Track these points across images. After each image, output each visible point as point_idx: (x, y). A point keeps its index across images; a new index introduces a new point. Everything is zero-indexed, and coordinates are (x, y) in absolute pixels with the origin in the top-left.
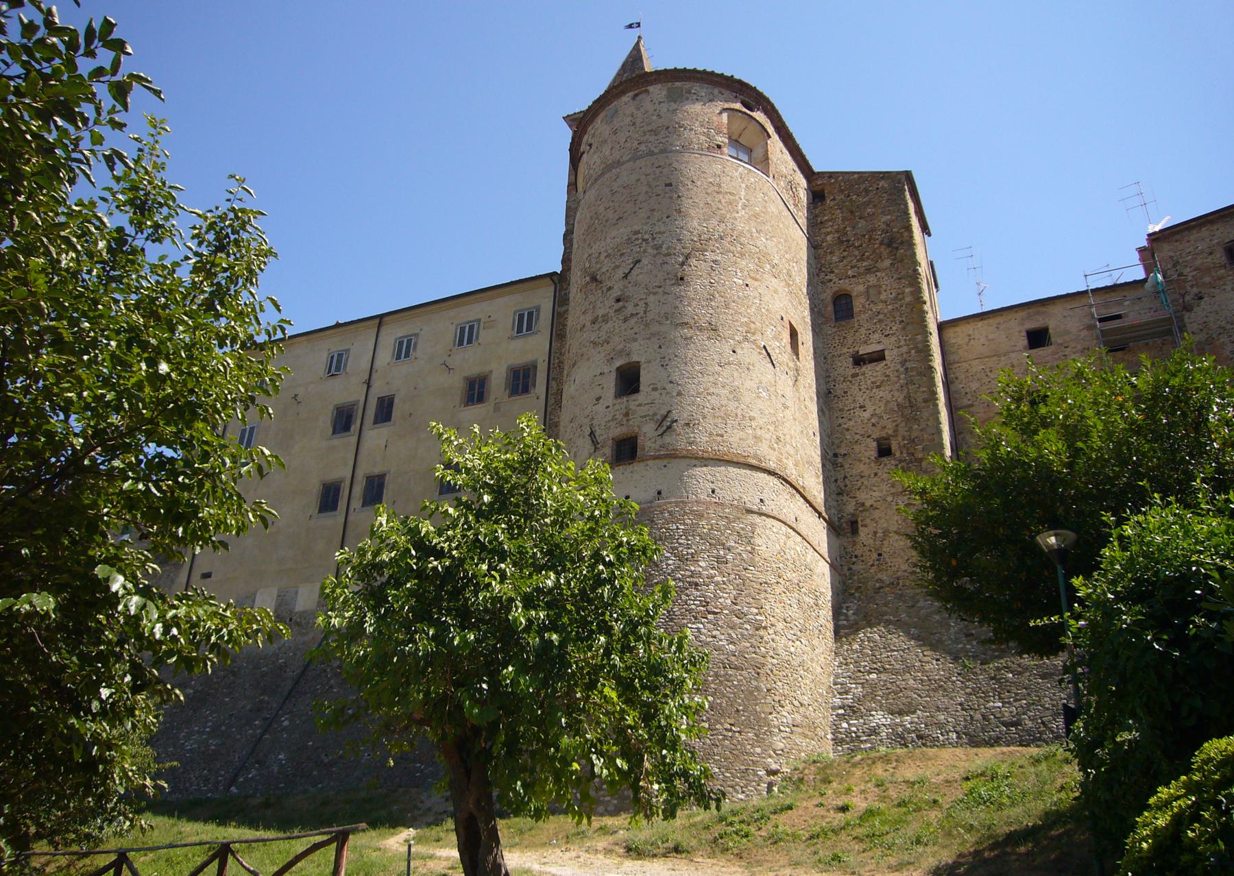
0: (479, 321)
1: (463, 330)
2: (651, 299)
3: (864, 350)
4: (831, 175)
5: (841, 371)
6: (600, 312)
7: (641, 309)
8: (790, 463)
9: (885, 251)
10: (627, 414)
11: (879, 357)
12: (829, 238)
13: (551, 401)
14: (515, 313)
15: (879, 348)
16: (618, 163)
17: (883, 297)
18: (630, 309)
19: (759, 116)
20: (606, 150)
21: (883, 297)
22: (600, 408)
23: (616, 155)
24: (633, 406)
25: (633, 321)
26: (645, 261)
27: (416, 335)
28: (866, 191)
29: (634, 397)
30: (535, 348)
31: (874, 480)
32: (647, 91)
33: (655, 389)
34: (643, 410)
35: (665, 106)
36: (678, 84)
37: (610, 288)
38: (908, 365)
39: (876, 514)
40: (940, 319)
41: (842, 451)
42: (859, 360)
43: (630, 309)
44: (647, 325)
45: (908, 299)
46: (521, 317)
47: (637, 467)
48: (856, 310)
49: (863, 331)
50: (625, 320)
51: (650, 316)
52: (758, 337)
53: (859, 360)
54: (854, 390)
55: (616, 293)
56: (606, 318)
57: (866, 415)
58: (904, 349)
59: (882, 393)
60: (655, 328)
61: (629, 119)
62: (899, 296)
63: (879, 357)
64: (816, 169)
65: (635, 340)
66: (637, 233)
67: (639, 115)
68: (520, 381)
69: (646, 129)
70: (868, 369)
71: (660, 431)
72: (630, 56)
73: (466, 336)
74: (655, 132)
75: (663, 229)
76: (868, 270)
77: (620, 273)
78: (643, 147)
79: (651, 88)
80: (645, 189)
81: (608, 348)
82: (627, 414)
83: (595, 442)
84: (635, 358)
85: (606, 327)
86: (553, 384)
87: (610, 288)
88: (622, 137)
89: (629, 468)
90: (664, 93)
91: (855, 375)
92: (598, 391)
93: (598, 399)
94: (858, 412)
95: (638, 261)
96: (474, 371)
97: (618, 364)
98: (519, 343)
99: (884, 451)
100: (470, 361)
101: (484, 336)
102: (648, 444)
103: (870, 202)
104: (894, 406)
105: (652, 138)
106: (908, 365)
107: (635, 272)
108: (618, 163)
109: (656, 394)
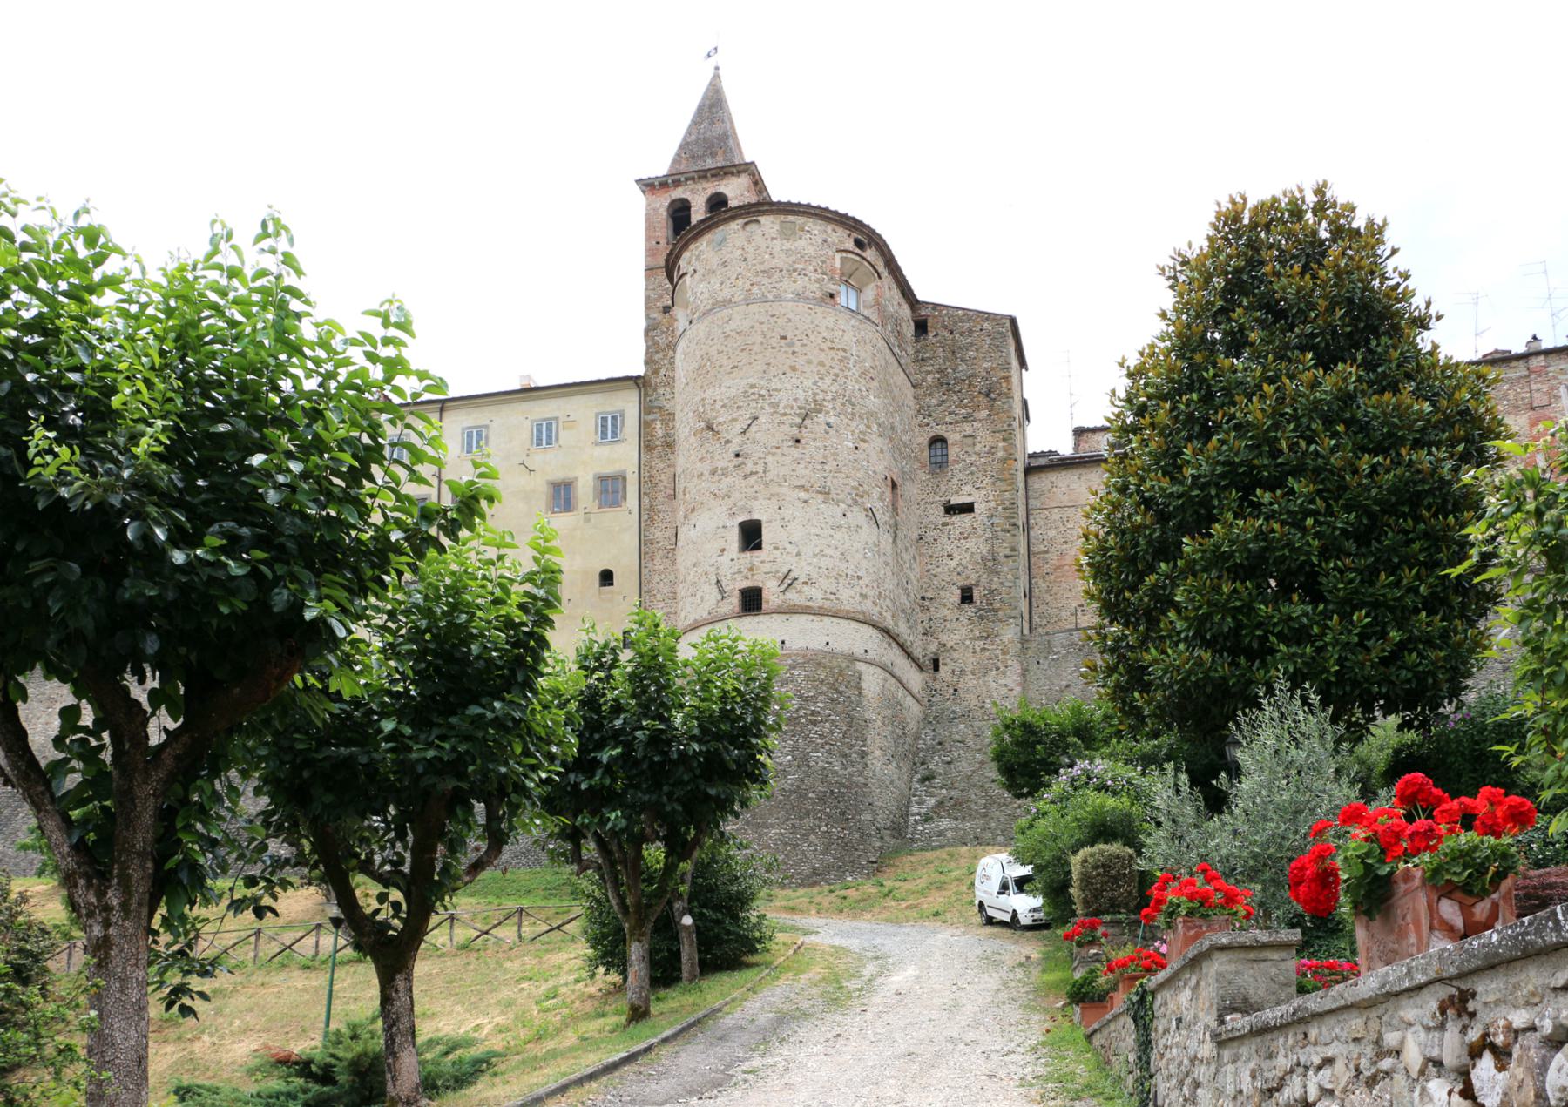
0: (557, 419)
1: (539, 427)
2: (770, 459)
3: (955, 500)
4: (935, 306)
5: (932, 518)
6: (720, 464)
7: (760, 468)
8: (888, 616)
9: (983, 400)
10: (751, 569)
11: (968, 508)
12: (929, 378)
13: (645, 517)
14: (597, 415)
15: (968, 500)
16: (728, 302)
17: (977, 449)
18: (749, 467)
19: (870, 254)
20: (715, 282)
21: (977, 449)
22: (725, 559)
23: (727, 293)
24: (756, 562)
25: (752, 479)
26: (762, 419)
27: (486, 427)
28: (970, 331)
29: (757, 553)
30: (624, 456)
31: (955, 624)
32: (757, 222)
33: (776, 548)
34: (767, 567)
35: (777, 243)
36: (791, 218)
37: (728, 442)
38: (995, 520)
39: (955, 655)
40: (1030, 451)
41: (929, 595)
42: (951, 509)
43: (749, 467)
44: (767, 485)
45: (1001, 454)
46: (604, 420)
47: (761, 618)
48: (951, 458)
49: (955, 481)
50: (745, 477)
51: (770, 476)
52: (866, 499)
53: (951, 509)
54: (944, 539)
55: (734, 448)
56: (725, 472)
57: (953, 564)
58: (993, 504)
59: (970, 545)
60: (775, 489)
61: (739, 252)
62: (992, 450)
63: (968, 508)
64: (921, 297)
65: (756, 499)
66: (753, 386)
67: (751, 250)
68: (610, 488)
69: (759, 267)
70: (958, 519)
71: (783, 587)
72: (705, 97)
73: (545, 435)
74: (767, 273)
75: (779, 386)
76: (966, 419)
77: (738, 427)
78: (755, 290)
79: (762, 219)
80: (760, 339)
81: (730, 502)
82: (751, 569)
83: (721, 591)
84: (756, 517)
85: (726, 481)
86: (646, 500)
87: (728, 442)
88: (733, 271)
89: (756, 619)
90: (777, 227)
91: (945, 524)
92: (722, 544)
93: (723, 550)
94: (946, 560)
95: (756, 418)
96: (560, 475)
97: (741, 519)
98: (605, 450)
99: (967, 596)
100: (552, 465)
101: (565, 436)
102: (772, 598)
103: (972, 344)
104: (978, 557)
105: (766, 281)
106: (995, 520)
107: (753, 428)
108: (728, 302)
109: (777, 553)
